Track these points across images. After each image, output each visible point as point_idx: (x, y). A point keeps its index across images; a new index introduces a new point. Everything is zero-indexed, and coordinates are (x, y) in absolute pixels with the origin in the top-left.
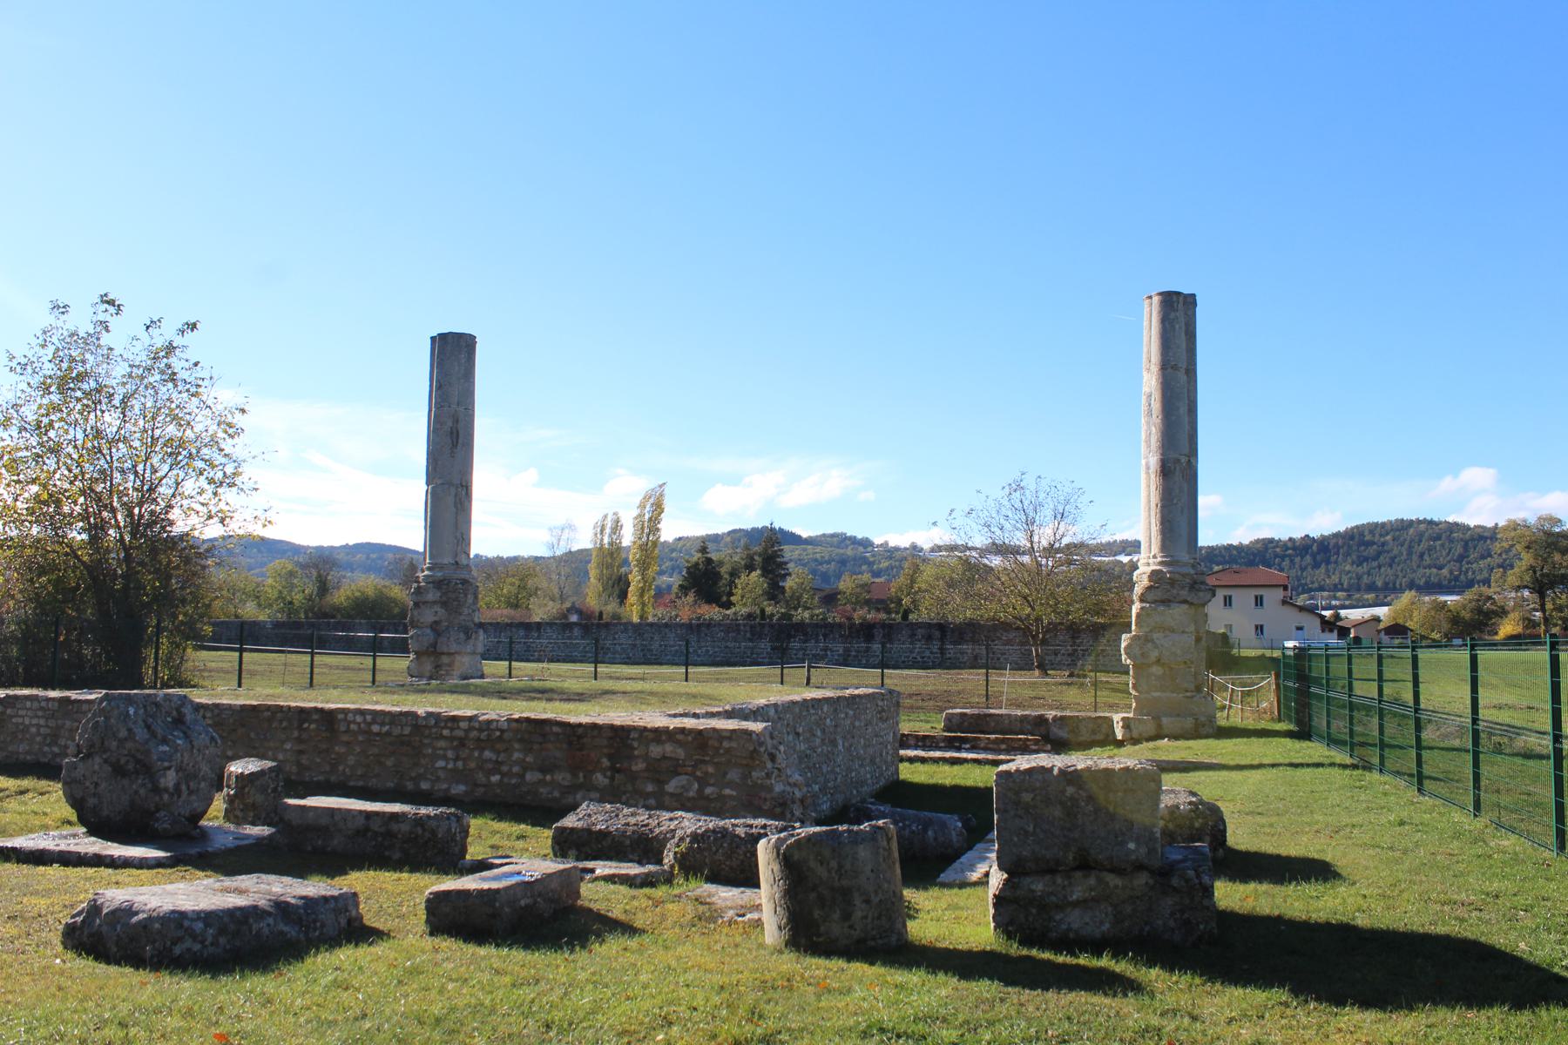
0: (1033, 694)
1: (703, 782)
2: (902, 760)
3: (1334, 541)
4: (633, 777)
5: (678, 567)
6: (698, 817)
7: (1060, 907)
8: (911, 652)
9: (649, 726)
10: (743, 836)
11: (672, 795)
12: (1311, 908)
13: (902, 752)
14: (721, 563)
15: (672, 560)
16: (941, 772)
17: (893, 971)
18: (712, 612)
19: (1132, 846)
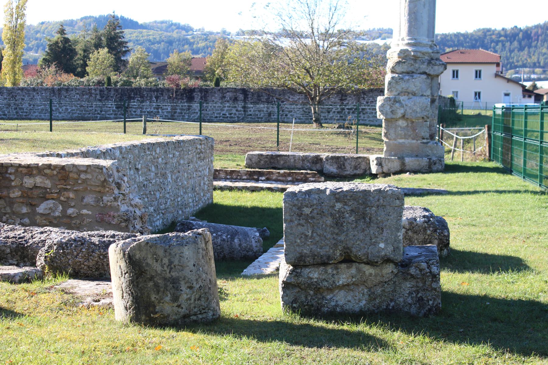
0: (312, 141)
1: (66, 204)
2: (215, 189)
3: (536, 30)
4: (11, 202)
5: (42, 45)
6: (63, 230)
7: (330, 290)
8: (222, 110)
9: (23, 163)
10: (97, 243)
11: (42, 215)
12: (508, 290)
13: (216, 183)
14: (76, 42)
15: (36, 39)
16: (244, 197)
17: (210, 337)
18: (68, 79)
19: (382, 245)
